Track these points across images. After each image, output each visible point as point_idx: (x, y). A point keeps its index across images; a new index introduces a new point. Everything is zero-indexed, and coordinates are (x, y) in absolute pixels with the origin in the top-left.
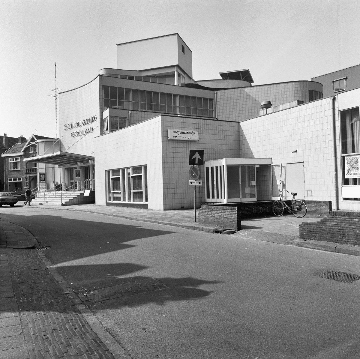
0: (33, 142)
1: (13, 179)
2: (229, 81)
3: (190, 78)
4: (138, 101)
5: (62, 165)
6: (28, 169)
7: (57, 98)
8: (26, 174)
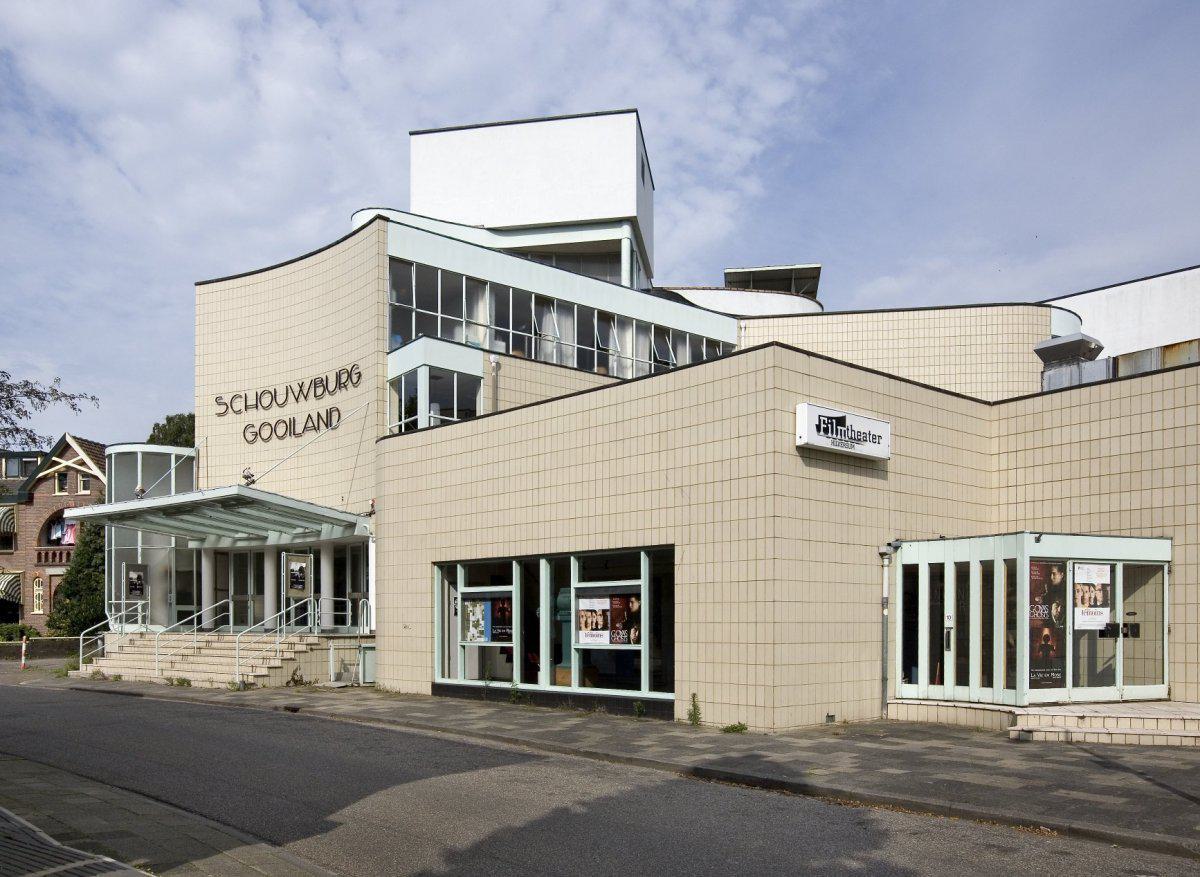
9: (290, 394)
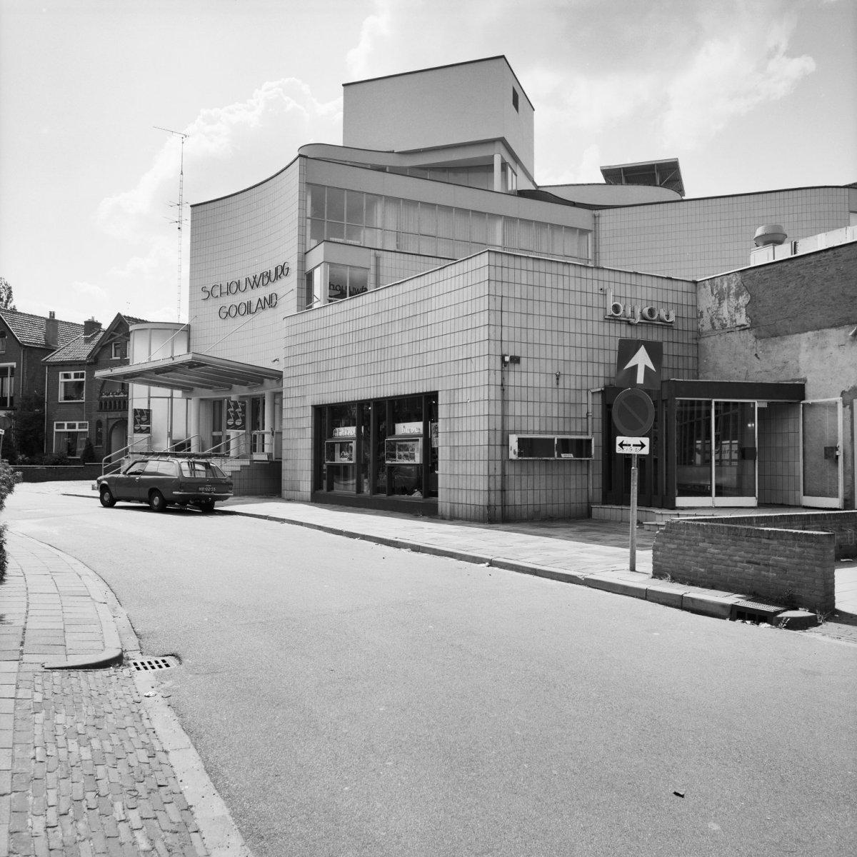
2: (624, 187)
3: (530, 178)
9: (248, 284)
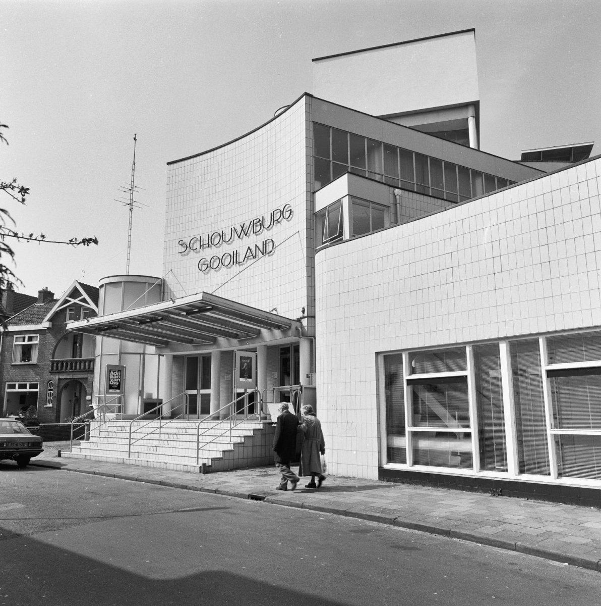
0: (75, 299)
1: (30, 385)
4: (398, 177)
5: (167, 344)
6: (58, 362)
7: (133, 207)
8: (52, 372)
